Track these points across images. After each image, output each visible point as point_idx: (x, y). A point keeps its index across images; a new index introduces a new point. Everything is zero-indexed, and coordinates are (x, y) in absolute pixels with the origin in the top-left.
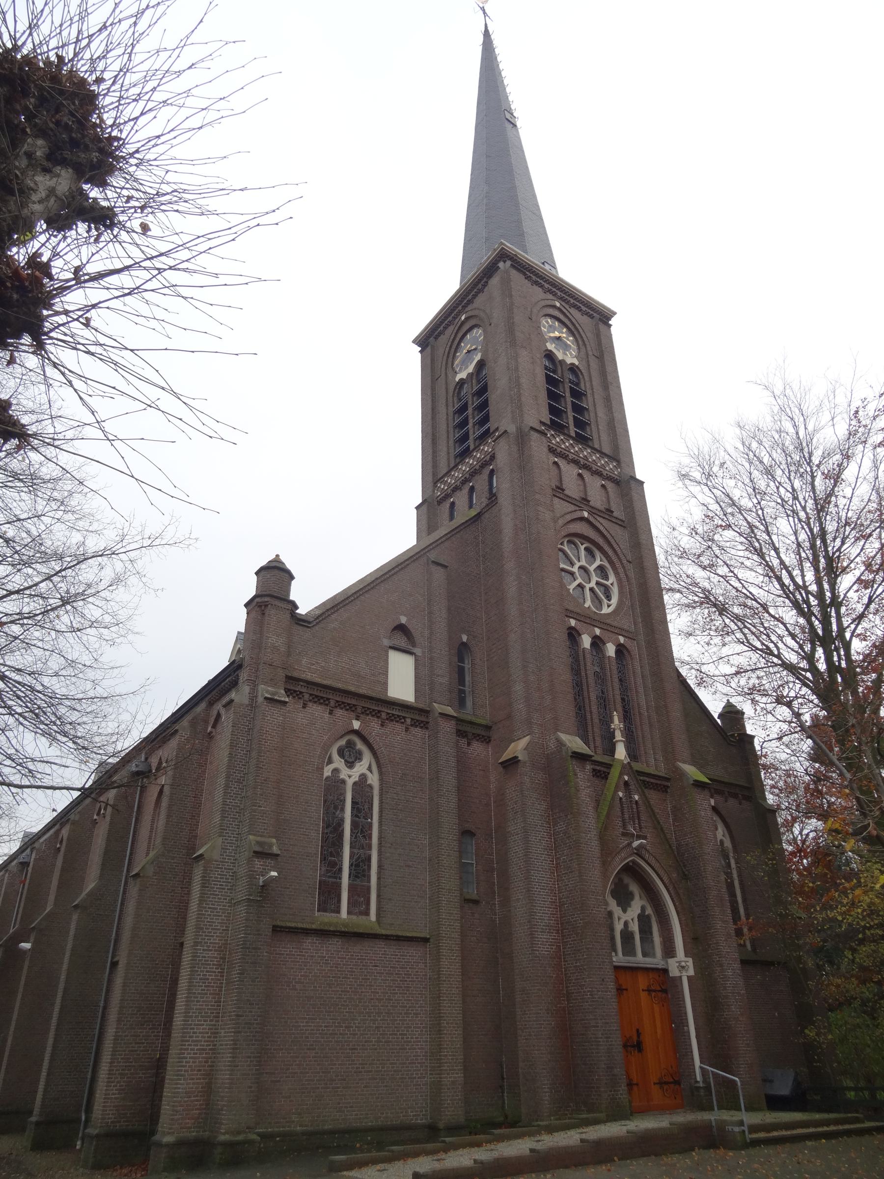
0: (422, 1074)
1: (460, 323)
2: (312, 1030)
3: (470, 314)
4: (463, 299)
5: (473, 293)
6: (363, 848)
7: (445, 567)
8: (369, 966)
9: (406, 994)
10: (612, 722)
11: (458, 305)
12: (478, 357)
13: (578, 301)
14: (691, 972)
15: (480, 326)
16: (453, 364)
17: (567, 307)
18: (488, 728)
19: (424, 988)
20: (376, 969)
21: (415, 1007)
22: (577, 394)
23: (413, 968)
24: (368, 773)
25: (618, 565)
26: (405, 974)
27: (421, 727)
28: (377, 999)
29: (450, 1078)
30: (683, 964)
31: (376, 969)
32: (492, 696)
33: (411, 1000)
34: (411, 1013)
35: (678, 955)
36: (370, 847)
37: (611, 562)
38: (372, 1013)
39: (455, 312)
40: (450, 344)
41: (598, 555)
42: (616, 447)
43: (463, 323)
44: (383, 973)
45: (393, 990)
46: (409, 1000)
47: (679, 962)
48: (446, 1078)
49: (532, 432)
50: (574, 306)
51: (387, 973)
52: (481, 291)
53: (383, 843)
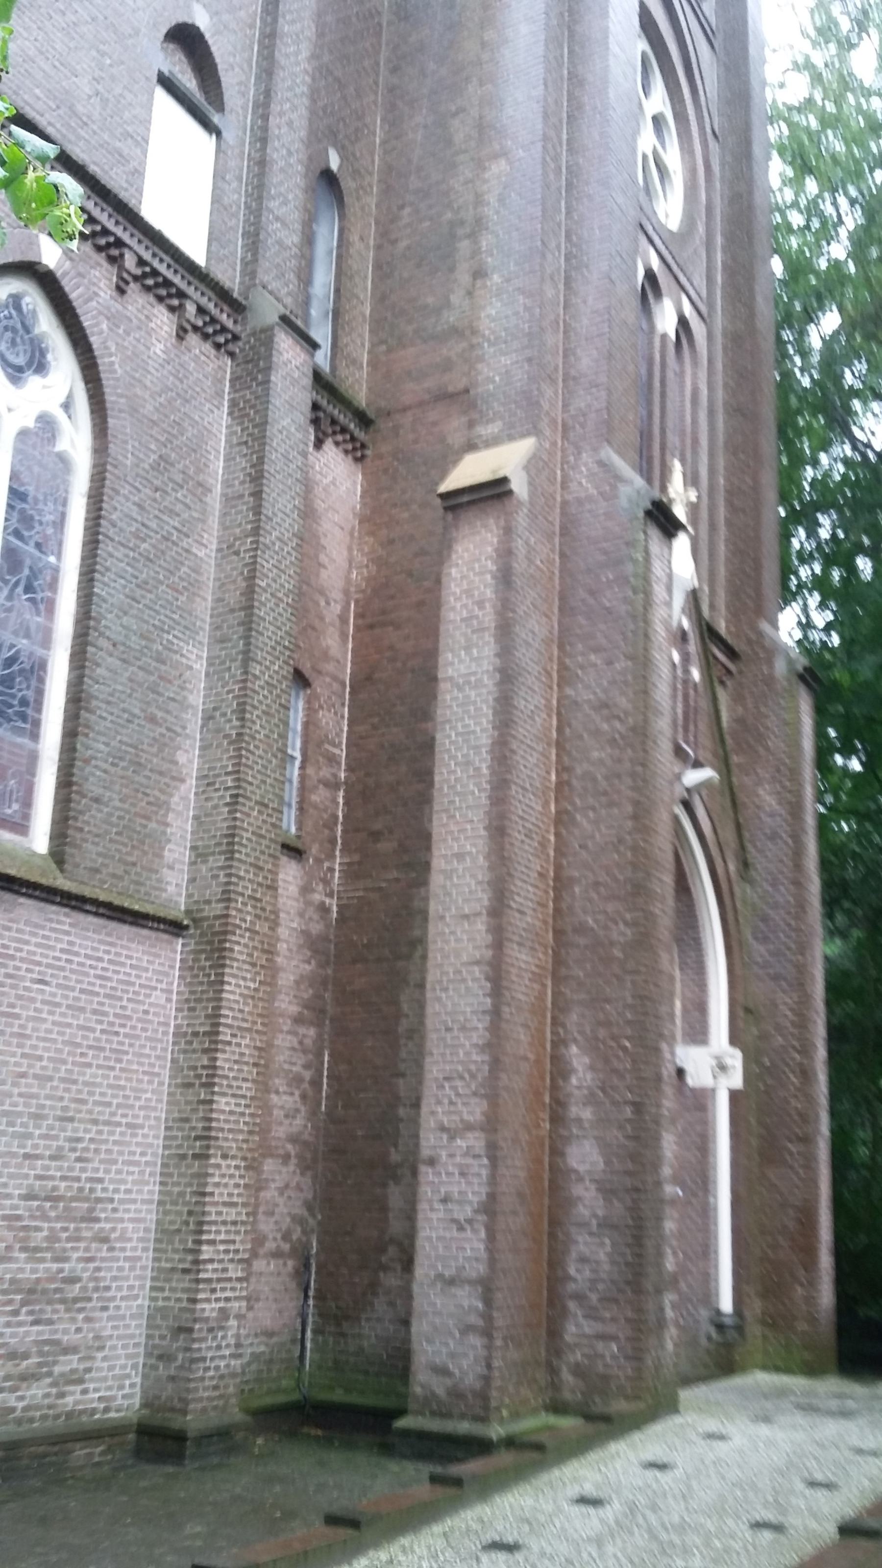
0: (131, 1288)
6: (27, 636)
8: (23, 978)
9: (113, 1068)
14: (736, 1080)
18: (364, 420)
19: (158, 1058)
20: (42, 991)
21: (132, 1107)
23: (139, 1002)
24: (61, 416)
26: (116, 1015)
27: (218, 346)
28: (36, 1076)
29: (217, 1300)
31: (42, 991)
32: (382, 342)
33: (123, 1088)
34: (119, 1124)
36: (47, 641)
37: (680, 117)
38: (20, 1114)
44: (58, 1005)
45: (82, 1055)
46: (119, 1087)
48: (208, 1300)
51: (69, 1007)
53: (93, 634)
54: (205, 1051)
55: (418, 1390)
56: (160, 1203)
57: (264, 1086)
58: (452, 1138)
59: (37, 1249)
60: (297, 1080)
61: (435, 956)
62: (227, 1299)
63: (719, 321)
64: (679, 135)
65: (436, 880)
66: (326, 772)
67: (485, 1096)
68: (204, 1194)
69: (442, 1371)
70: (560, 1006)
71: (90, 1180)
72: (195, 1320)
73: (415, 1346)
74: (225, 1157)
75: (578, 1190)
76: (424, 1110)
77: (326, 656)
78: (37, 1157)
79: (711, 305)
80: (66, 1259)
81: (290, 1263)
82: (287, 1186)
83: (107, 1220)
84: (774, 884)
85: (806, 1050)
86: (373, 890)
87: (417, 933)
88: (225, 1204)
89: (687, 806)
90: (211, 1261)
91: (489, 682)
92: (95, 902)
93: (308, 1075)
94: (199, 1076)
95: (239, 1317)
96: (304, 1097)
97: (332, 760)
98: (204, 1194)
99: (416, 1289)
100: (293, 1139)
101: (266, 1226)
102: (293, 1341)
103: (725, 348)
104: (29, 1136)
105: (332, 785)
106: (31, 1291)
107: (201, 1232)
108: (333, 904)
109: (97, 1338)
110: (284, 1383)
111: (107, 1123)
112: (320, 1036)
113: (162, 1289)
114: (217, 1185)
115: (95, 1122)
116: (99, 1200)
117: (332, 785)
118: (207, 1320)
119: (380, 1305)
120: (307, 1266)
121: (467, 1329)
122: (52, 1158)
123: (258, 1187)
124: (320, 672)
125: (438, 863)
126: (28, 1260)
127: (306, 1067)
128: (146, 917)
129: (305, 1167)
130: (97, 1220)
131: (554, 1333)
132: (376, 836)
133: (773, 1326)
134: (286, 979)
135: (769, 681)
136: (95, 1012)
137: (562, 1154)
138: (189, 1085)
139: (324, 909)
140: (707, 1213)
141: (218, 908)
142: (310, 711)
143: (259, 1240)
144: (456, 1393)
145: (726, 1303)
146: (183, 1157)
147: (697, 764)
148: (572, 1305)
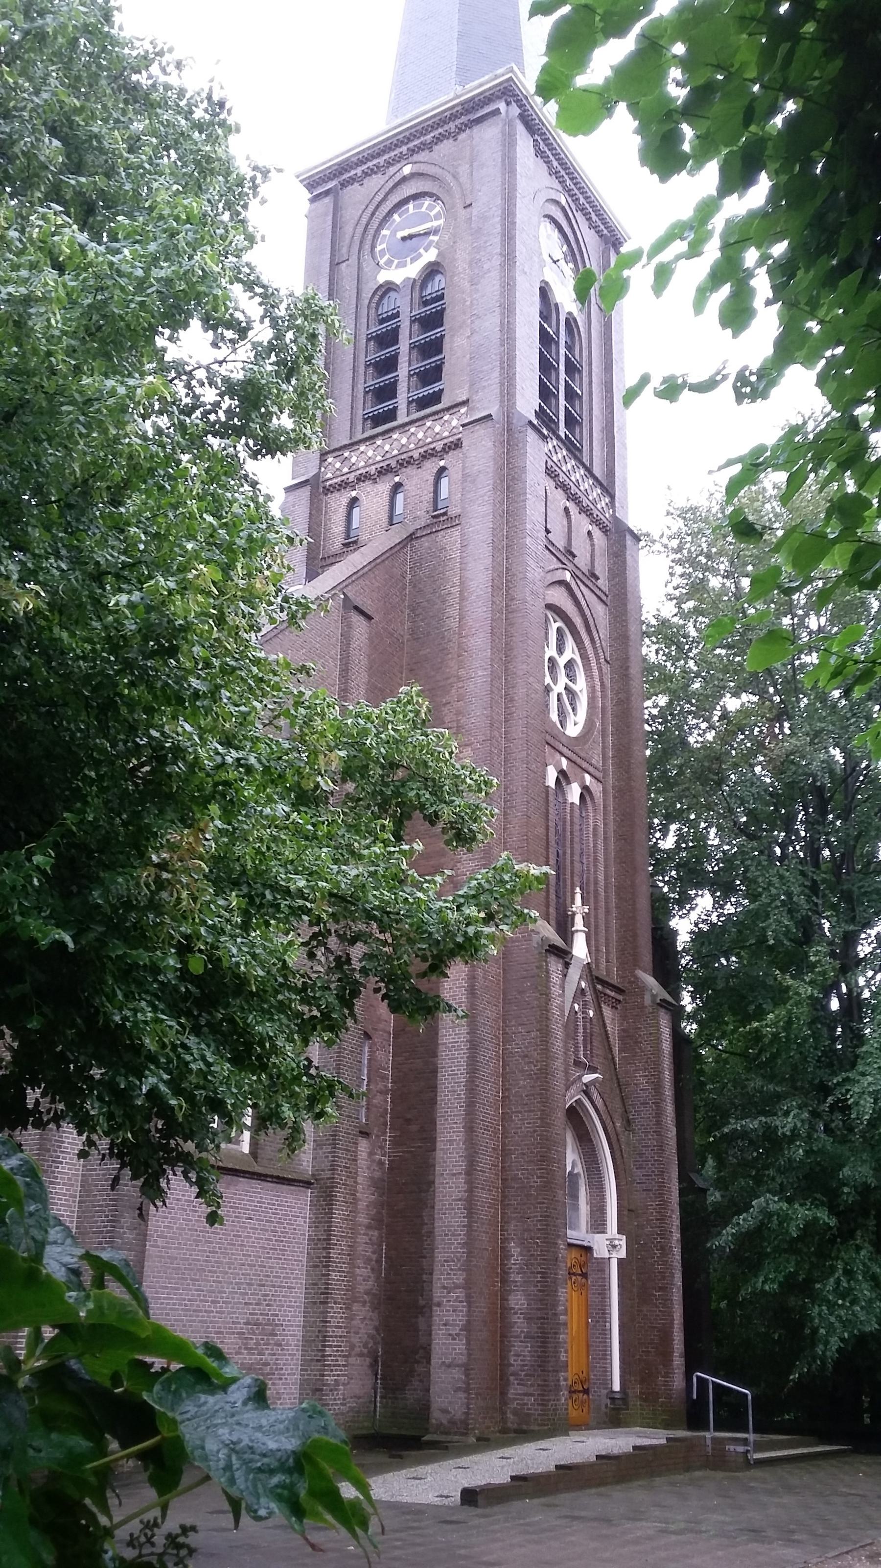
1: (398, 177)
2: (174, 1304)
3: (422, 168)
4: (414, 137)
5: (436, 133)
7: (369, 618)
10: (573, 902)
11: (401, 143)
12: (431, 256)
13: (589, 203)
14: (623, 1254)
15: (438, 198)
16: (373, 247)
17: (573, 207)
22: (572, 368)
25: (594, 664)
28: (249, 1265)
30: (617, 1242)
35: (609, 1230)
37: (584, 657)
39: (392, 154)
40: (371, 208)
41: (570, 642)
42: (611, 473)
43: (405, 179)
47: (611, 1240)
48: (329, 1375)
49: (530, 431)
50: (586, 215)
52: (452, 136)
54: (324, 1249)
55: (434, 1421)
56: (304, 1327)
57: (353, 1265)
58: (449, 1292)
59: (251, 1349)
60: (368, 1260)
61: (439, 1196)
62: (338, 1375)
63: (610, 781)
64: (585, 670)
65: (439, 1154)
66: (380, 1086)
67: (464, 1270)
68: (327, 1322)
69: (445, 1411)
70: (505, 1221)
71: (272, 1315)
72: (324, 1385)
73: (432, 1399)
74: (335, 1303)
75: (514, 1319)
76: (435, 1277)
77: (380, 1020)
78: (251, 1304)
79: (605, 771)
80: (264, 1354)
81: (368, 1359)
82: (365, 1318)
83: (281, 1335)
84: (646, 1133)
85: (665, 1234)
86: (408, 1152)
87: (431, 1177)
88: (336, 1327)
89: (586, 1093)
90: (330, 1356)
91: (465, 1047)
92: (272, 1176)
93: (374, 1257)
94: (321, 1262)
95: (344, 1384)
96: (372, 1269)
97: (384, 1078)
98: (327, 1322)
99: (432, 1370)
100: (367, 1293)
101: (355, 1340)
102: (370, 1402)
103: (615, 797)
104: (247, 1294)
105: (384, 1092)
106: (250, 1369)
107: (325, 1341)
108: (386, 1160)
109: (278, 1393)
110: (366, 1424)
111: (279, 1287)
112: (381, 1236)
113: (306, 1370)
114: (332, 1317)
115: (274, 1286)
116: (277, 1325)
117: (384, 1092)
118: (329, 1385)
119: (416, 1383)
120: (376, 1361)
121: (458, 1389)
122: (257, 1304)
123: (350, 1318)
124: (376, 1030)
125: (440, 1145)
126: (248, 1354)
127: (373, 1253)
128: (294, 1180)
129: (374, 1308)
130: (276, 1335)
131: (503, 1394)
132: (408, 1121)
133: (645, 1400)
134: (362, 1205)
135: (642, 1007)
136: (272, 1231)
137: (507, 1300)
138: (318, 1266)
139: (381, 1163)
140: (606, 1334)
141: (328, 1174)
142: (372, 1052)
143: (352, 1347)
144: (452, 1422)
145: (617, 1387)
146: (315, 1303)
147: (593, 1070)
148: (512, 1378)
